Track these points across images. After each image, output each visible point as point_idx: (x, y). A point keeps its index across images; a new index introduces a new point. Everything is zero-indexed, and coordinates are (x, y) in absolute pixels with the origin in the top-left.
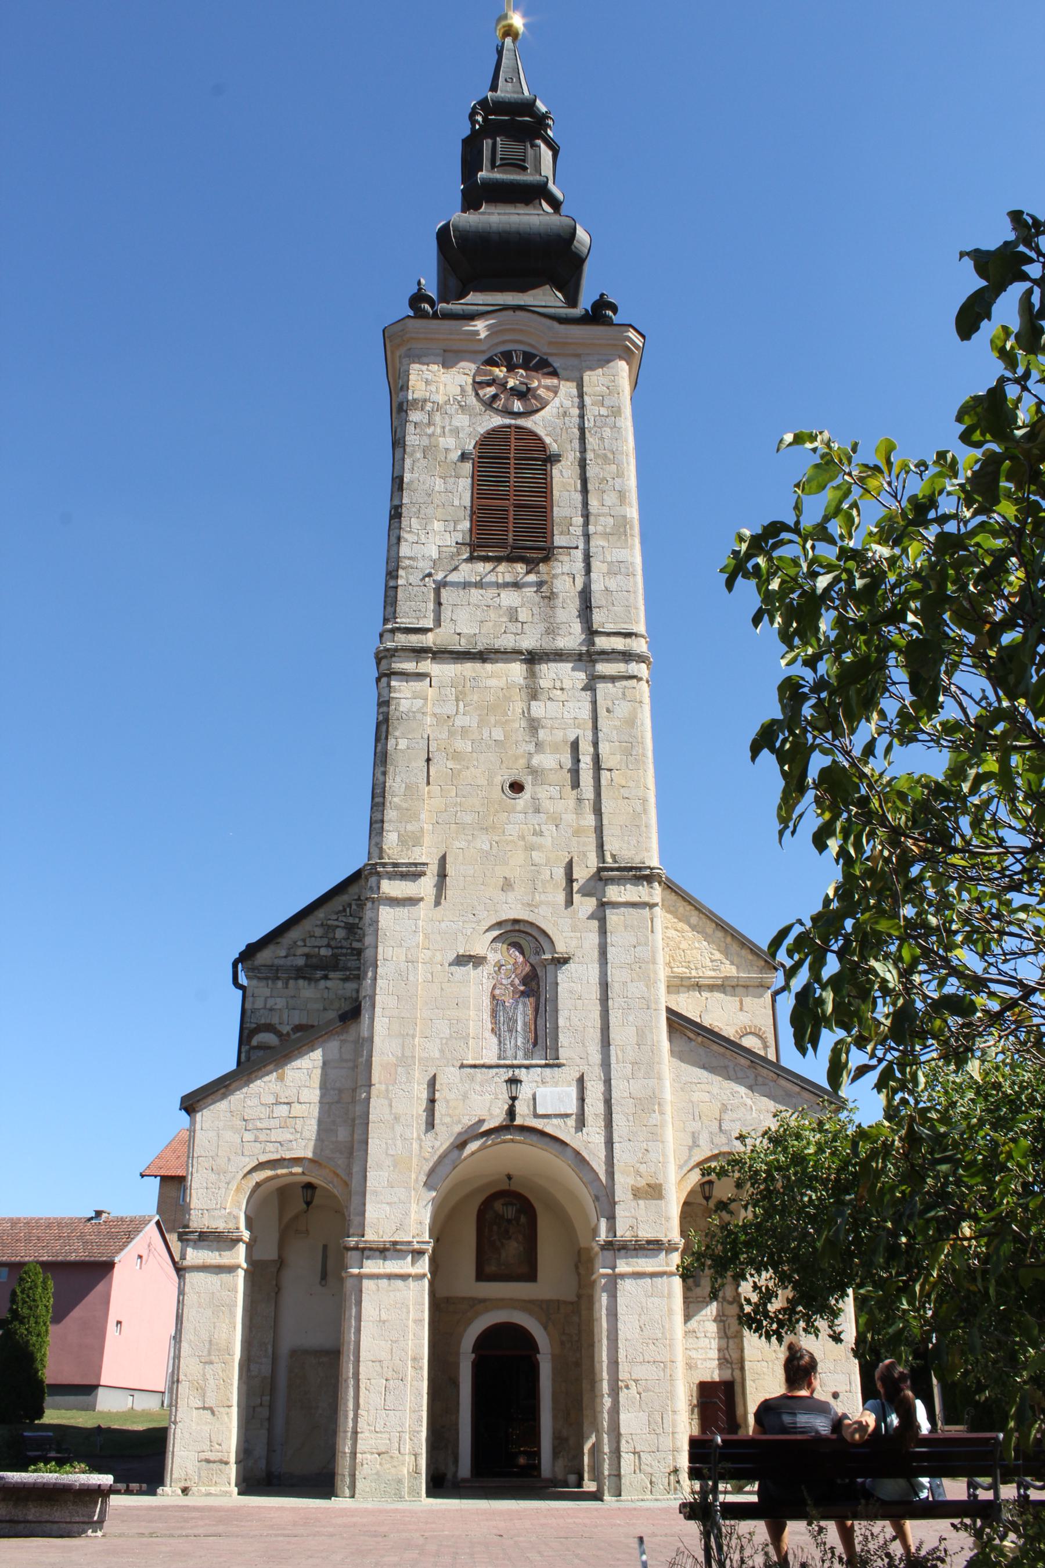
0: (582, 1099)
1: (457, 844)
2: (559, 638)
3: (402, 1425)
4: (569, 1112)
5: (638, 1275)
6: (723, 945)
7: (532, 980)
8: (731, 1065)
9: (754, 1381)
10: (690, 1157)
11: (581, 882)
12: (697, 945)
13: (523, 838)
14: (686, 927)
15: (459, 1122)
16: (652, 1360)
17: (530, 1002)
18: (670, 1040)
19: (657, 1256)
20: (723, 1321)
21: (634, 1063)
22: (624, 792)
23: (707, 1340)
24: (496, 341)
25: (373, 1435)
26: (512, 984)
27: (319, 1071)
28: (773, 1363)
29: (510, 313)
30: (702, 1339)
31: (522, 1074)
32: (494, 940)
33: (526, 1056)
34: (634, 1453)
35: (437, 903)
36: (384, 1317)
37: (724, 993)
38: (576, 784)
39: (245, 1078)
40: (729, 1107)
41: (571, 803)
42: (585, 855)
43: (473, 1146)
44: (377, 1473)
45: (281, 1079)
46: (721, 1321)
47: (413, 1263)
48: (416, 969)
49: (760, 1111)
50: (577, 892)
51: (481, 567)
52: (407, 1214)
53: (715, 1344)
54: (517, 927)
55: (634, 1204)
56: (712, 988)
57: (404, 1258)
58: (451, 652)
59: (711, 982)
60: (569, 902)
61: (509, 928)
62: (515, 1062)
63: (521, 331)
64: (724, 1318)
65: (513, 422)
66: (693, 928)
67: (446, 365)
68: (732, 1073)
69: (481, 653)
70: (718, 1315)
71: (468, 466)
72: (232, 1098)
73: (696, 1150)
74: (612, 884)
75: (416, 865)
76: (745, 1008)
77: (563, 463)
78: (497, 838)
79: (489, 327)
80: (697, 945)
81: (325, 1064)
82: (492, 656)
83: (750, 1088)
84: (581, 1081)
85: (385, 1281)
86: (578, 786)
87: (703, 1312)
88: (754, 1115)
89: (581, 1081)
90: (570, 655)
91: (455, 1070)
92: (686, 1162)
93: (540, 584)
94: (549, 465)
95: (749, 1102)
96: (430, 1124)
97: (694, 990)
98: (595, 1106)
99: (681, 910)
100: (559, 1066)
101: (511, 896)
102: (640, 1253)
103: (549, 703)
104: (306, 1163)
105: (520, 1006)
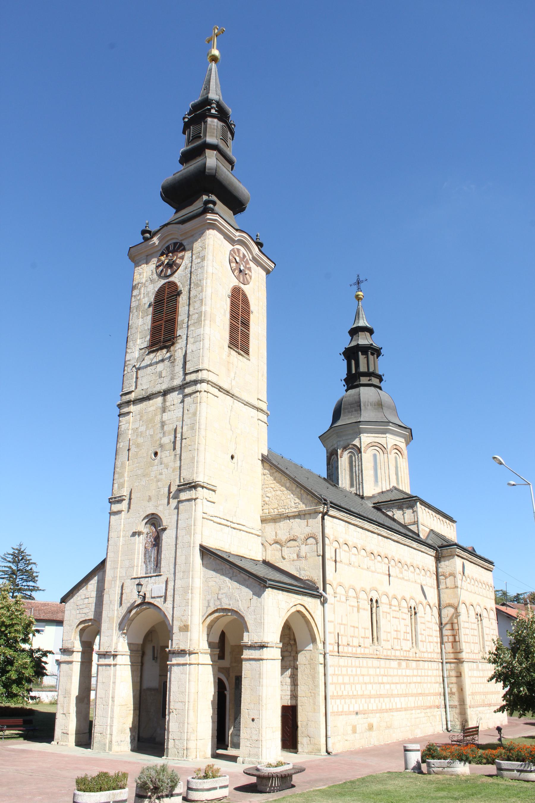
0: (166, 590)
1: (136, 484)
2: (175, 380)
3: (107, 723)
4: (162, 595)
5: (178, 665)
6: (300, 495)
7: (157, 539)
8: (224, 568)
9: (301, 706)
10: (207, 611)
11: (173, 493)
12: (289, 497)
13: (156, 477)
14: (284, 489)
15: (129, 602)
16: (181, 701)
17: (156, 548)
18: (202, 559)
19: (185, 656)
20: (293, 678)
21: (183, 572)
22: (189, 448)
23: (286, 686)
24: (164, 242)
25: (99, 726)
26: (151, 541)
27: (96, 584)
28: (310, 698)
29: (165, 228)
30: (284, 686)
31: (143, 581)
32: (146, 524)
33: (154, 572)
34: (173, 740)
35: (128, 511)
36: (104, 681)
37: (301, 519)
38: (174, 449)
39: (77, 589)
40: (222, 588)
41: (173, 457)
42: (175, 480)
43: (134, 612)
44: (99, 741)
45: (87, 589)
46: (293, 677)
47: (114, 659)
48: (119, 540)
49: (233, 589)
50: (171, 498)
51: (152, 355)
52: (112, 640)
53: (289, 688)
54: (153, 517)
55: (179, 634)
56: (294, 517)
57: (110, 658)
58: (138, 399)
59: (293, 514)
60: (169, 503)
61: (151, 517)
62: (150, 575)
63: (169, 235)
64: (294, 676)
65: (168, 280)
66: (287, 489)
67: (147, 263)
68: (224, 572)
69: (148, 396)
70: (291, 675)
71: (151, 309)
72: (74, 597)
73: (209, 608)
74: (182, 492)
75: (120, 496)
76: (309, 525)
77: (183, 293)
78: (148, 479)
79: (159, 239)
80: (289, 497)
81: (98, 581)
82: (152, 397)
83: (231, 578)
84: (167, 582)
85: (105, 667)
86: (175, 449)
87: (285, 673)
88: (231, 590)
89: (167, 582)
90: (177, 388)
91: (129, 580)
92: (205, 613)
93: (170, 357)
94: (178, 297)
95: (229, 585)
96: (121, 604)
97: (287, 519)
98: (170, 592)
99: (283, 481)
100: (160, 575)
101: (151, 503)
102: (180, 655)
103: (169, 412)
104: (93, 621)
105: (153, 550)
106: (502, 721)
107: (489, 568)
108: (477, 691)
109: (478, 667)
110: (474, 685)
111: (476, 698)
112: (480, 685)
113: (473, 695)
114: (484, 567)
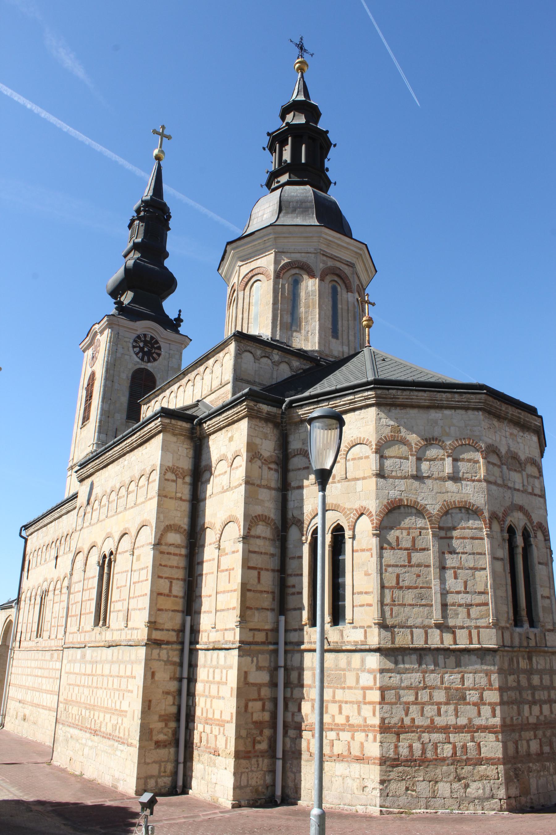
106: (118, 780)
107: (147, 437)
108: (74, 699)
109: (84, 656)
110: (71, 687)
111: (70, 711)
112: (81, 689)
113: (67, 704)
114: (135, 445)
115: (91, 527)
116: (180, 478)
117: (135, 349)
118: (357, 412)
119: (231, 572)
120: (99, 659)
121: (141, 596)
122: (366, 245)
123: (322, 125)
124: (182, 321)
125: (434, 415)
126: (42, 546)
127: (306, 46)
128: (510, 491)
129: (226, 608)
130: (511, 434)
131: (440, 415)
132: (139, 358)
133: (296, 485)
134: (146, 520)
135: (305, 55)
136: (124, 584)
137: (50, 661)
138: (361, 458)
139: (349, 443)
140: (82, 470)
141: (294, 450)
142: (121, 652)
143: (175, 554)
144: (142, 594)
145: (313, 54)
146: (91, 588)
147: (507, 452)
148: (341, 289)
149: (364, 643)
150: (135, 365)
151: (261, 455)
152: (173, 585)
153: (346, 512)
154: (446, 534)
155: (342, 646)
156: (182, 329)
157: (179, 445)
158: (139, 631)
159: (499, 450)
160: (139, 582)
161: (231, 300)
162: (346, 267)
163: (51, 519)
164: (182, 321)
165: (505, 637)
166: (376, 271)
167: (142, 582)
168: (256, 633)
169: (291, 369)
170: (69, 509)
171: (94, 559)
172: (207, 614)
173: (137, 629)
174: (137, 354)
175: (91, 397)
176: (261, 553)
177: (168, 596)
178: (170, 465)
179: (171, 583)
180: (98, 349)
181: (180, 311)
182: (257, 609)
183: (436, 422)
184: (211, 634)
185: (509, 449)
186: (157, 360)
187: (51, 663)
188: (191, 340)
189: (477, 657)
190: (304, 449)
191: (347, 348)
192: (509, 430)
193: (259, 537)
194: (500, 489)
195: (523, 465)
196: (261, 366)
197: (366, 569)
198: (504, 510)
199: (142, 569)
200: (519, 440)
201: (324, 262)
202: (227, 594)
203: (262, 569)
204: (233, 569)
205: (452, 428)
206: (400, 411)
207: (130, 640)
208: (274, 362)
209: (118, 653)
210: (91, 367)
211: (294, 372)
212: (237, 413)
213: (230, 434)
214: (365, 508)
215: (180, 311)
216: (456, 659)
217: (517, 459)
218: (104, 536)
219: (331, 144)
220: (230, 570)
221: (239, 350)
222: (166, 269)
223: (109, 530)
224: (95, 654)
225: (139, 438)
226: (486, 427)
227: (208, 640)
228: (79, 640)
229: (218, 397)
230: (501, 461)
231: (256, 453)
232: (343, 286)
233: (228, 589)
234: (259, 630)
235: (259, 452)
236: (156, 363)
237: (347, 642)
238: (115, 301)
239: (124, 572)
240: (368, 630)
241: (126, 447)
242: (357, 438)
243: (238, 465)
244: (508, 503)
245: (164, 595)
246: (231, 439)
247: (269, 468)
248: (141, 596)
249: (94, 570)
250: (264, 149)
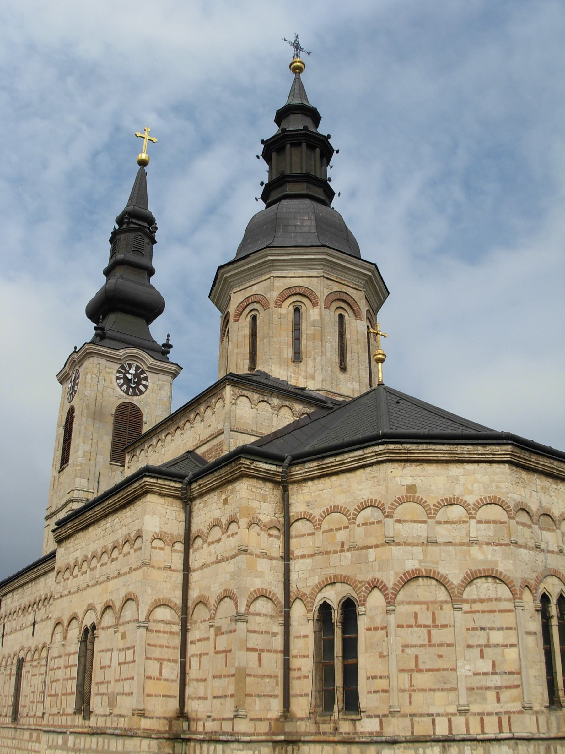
109: (65, 742)
114: (117, 506)
115: (70, 596)
116: (168, 545)
117: (119, 381)
118: (368, 470)
119: (228, 654)
120: (82, 746)
121: (128, 679)
122: (375, 265)
123: (322, 129)
124: (171, 346)
125: (455, 470)
126: (18, 609)
127: (302, 45)
128: (542, 553)
129: (223, 695)
130: (543, 488)
131: (462, 470)
132: (123, 391)
133: (300, 554)
134: (131, 593)
135: (302, 54)
136: (108, 664)
137: (29, 741)
138: (373, 523)
139: (358, 506)
140: (60, 530)
141: (297, 513)
142: (106, 741)
143: (164, 632)
144: (129, 677)
145: (309, 55)
146: (72, 666)
147: (538, 509)
148: (349, 318)
149: (380, 734)
150: (119, 399)
151: (259, 520)
152: (163, 666)
153: (357, 585)
154: (471, 608)
155: (355, 738)
156: (172, 356)
157: (167, 507)
158: (126, 719)
159: (530, 507)
160: (125, 663)
161: (225, 331)
162: (354, 291)
163: (27, 580)
164: (171, 346)
165: (539, 723)
166: (389, 293)
167: (128, 663)
168: (258, 723)
169: (293, 414)
170: (47, 569)
171: (75, 633)
172: (202, 701)
173: (124, 716)
174: (121, 386)
175: (70, 436)
176: (262, 632)
177: (158, 679)
178: (158, 530)
179: (161, 664)
180: (77, 381)
181: (169, 336)
182: (259, 696)
183: (456, 479)
184: (207, 724)
185: (541, 506)
186: (144, 393)
187: (30, 744)
188: (182, 368)
189: (509, 747)
190: (308, 513)
191: (358, 384)
192: (540, 483)
193: (259, 614)
194: (531, 552)
195: (557, 522)
196: (259, 412)
197: (380, 650)
198: (537, 577)
199: (129, 648)
200: (552, 494)
201: (328, 287)
202: (223, 679)
203: (262, 650)
204: (230, 651)
205: (476, 485)
206: (415, 467)
207: (116, 728)
208: (274, 407)
209: (104, 742)
210: (70, 402)
211: (297, 417)
212: (231, 473)
213: (224, 497)
214: (378, 580)
215: (169, 336)
216: (484, 750)
217: (550, 516)
218: (85, 607)
219: (334, 150)
220: (227, 651)
221: (233, 395)
222: (153, 287)
223: (91, 601)
224: (78, 741)
225: (123, 499)
226: (514, 482)
227: (204, 730)
228: (60, 724)
229: (211, 449)
230: (532, 520)
231: (253, 518)
232: (351, 313)
233: (225, 673)
234: (261, 720)
235: (257, 517)
236: (143, 396)
237: (361, 732)
238: (96, 325)
239: (108, 650)
240: (384, 719)
241: (108, 508)
242: (368, 500)
243: (234, 532)
244: (541, 569)
245: (154, 679)
246: (225, 502)
247: (269, 535)
248: (128, 679)
249: (74, 647)
250: (258, 157)
